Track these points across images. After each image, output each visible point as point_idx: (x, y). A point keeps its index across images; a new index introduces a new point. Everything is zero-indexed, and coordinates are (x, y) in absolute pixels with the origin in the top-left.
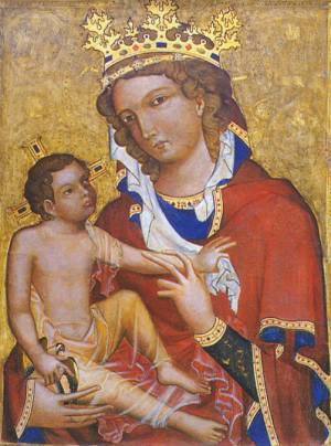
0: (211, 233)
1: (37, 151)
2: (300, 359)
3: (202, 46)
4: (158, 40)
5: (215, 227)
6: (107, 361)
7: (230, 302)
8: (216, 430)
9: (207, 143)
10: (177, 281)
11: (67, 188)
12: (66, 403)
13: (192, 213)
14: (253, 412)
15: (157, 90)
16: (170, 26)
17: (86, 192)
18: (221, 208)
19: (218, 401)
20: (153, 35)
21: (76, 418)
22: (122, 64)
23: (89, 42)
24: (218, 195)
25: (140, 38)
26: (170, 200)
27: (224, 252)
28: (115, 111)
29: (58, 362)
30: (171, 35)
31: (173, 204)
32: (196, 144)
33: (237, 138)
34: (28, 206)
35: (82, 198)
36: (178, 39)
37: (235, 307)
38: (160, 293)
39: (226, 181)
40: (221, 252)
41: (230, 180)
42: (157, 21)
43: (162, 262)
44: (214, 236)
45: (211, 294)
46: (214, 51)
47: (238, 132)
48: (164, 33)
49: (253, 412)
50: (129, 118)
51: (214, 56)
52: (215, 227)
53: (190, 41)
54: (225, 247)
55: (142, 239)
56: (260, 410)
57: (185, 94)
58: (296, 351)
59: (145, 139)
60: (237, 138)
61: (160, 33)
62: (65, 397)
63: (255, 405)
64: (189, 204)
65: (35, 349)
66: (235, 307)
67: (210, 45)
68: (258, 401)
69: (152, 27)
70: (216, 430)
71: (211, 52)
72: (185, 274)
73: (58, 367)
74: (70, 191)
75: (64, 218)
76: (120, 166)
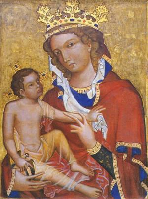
0: (95, 104)
1: (17, 67)
2: (134, 160)
3: (90, 20)
4: (71, 18)
5: (96, 101)
6: (48, 161)
7: (103, 135)
8: (97, 192)
9: (92, 64)
10: (79, 125)
11: (30, 84)
12: (29, 180)
13: (86, 95)
14: (113, 184)
16: (76, 12)
17: (38, 86)
18: (99, 93)
19: (98, 179)
20: (68, 16)
21: (34, 187)
22: (55, 28)
23: (40, 19)
24: (98, 87)
25: (63, 17)
26: (76, 89)
27: (100, 112)
28: (51, 49)
29: (26, 162)
30: (77, 16)
31: (78, 91)
32: (88, 64)
33: (106, 62)
34: (12, 92)
35: (36, 88)
36: (80, 17)
37: (105, 137)
38: (72, 131)
39: (101, 81)
40: (99, 112)
41: (103, 80)
42: (70, 10)
43: (72, 117)
44: (96, 105)
45: (94, 131)
46: (96, 23)
47: (106, 59)
48: (73, 15)
49: (113, 184)
50: (58, 53)
51: (95, 25)
52: (96, 101)
53: (85, 18)
54: (100, 110)
55: (64, 107)
56: (116, 183)
57: (83, 42)
58: (132, 156)
59: (65, 62)
60: (106, 62)
61: (71, 15)
62: (29, 177)
63: (114, 181)
64: (85, 91)
65: (16, 156)
66: (105, 137)
67: (94, 20)
68: (115, 179)
69: (68, 12)
70: (97, 192)
71: (94, 23)
72: (83, 122)
73: (26, 164)
74: (31, 85)
75: (29, 97)
76: (54, 74)
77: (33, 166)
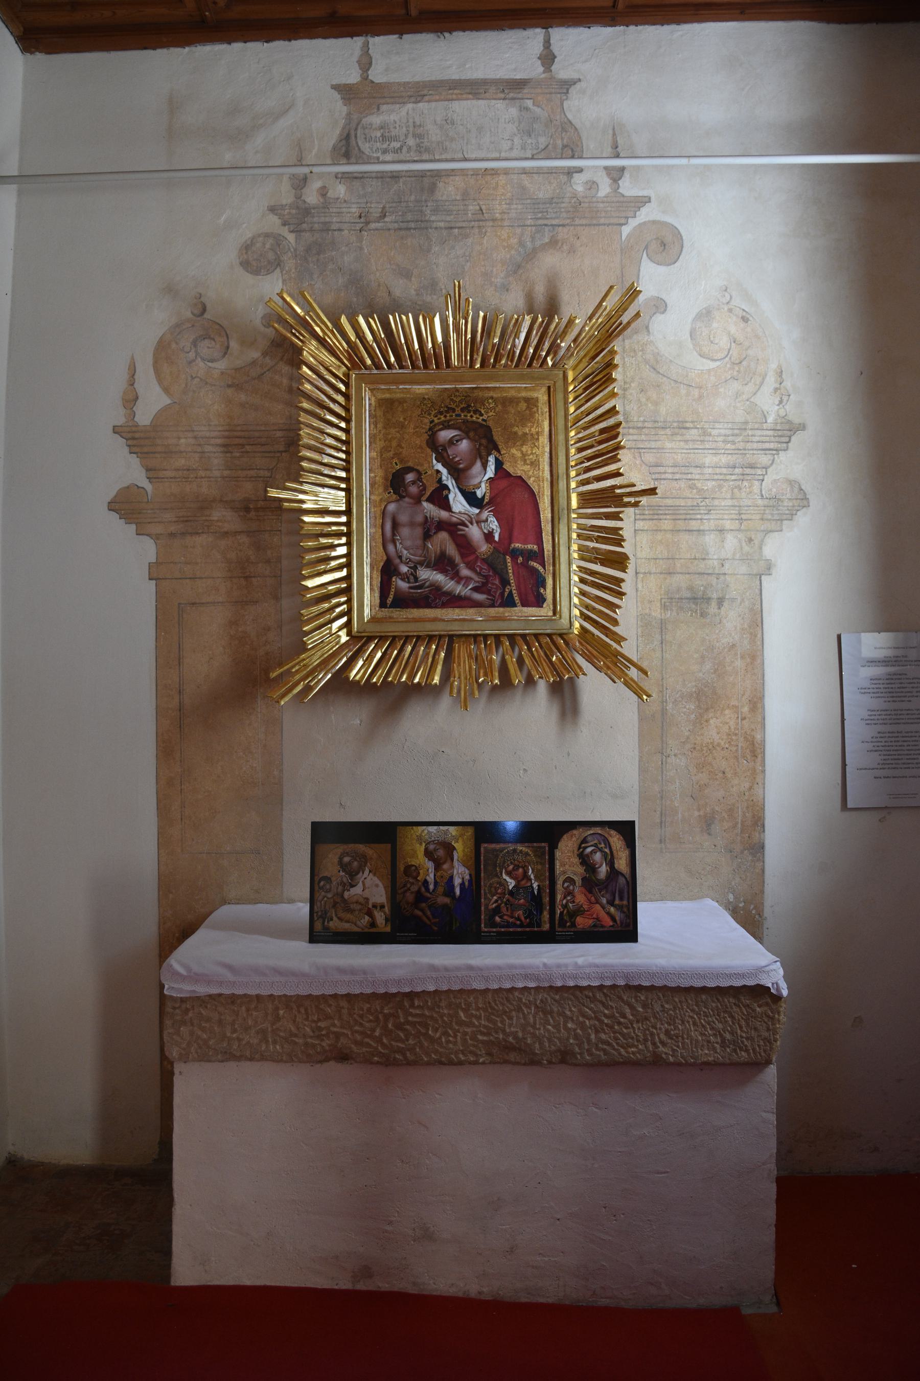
5: (486, 501)
7: (494, 537)
10: (467, 526)
12: (410, 588)
13: (475, 493)
21: (414, 595)
30: (462, 410)
37: (497, 538)
45: (484, 533)
52: (486, 501)
55: (450, 505)
57: (468, 438)
62: (412, 585)
65: (397, 561)
66: (497, 538)
68: (510, 586)
72: (472, 524)
76: (438, 472)
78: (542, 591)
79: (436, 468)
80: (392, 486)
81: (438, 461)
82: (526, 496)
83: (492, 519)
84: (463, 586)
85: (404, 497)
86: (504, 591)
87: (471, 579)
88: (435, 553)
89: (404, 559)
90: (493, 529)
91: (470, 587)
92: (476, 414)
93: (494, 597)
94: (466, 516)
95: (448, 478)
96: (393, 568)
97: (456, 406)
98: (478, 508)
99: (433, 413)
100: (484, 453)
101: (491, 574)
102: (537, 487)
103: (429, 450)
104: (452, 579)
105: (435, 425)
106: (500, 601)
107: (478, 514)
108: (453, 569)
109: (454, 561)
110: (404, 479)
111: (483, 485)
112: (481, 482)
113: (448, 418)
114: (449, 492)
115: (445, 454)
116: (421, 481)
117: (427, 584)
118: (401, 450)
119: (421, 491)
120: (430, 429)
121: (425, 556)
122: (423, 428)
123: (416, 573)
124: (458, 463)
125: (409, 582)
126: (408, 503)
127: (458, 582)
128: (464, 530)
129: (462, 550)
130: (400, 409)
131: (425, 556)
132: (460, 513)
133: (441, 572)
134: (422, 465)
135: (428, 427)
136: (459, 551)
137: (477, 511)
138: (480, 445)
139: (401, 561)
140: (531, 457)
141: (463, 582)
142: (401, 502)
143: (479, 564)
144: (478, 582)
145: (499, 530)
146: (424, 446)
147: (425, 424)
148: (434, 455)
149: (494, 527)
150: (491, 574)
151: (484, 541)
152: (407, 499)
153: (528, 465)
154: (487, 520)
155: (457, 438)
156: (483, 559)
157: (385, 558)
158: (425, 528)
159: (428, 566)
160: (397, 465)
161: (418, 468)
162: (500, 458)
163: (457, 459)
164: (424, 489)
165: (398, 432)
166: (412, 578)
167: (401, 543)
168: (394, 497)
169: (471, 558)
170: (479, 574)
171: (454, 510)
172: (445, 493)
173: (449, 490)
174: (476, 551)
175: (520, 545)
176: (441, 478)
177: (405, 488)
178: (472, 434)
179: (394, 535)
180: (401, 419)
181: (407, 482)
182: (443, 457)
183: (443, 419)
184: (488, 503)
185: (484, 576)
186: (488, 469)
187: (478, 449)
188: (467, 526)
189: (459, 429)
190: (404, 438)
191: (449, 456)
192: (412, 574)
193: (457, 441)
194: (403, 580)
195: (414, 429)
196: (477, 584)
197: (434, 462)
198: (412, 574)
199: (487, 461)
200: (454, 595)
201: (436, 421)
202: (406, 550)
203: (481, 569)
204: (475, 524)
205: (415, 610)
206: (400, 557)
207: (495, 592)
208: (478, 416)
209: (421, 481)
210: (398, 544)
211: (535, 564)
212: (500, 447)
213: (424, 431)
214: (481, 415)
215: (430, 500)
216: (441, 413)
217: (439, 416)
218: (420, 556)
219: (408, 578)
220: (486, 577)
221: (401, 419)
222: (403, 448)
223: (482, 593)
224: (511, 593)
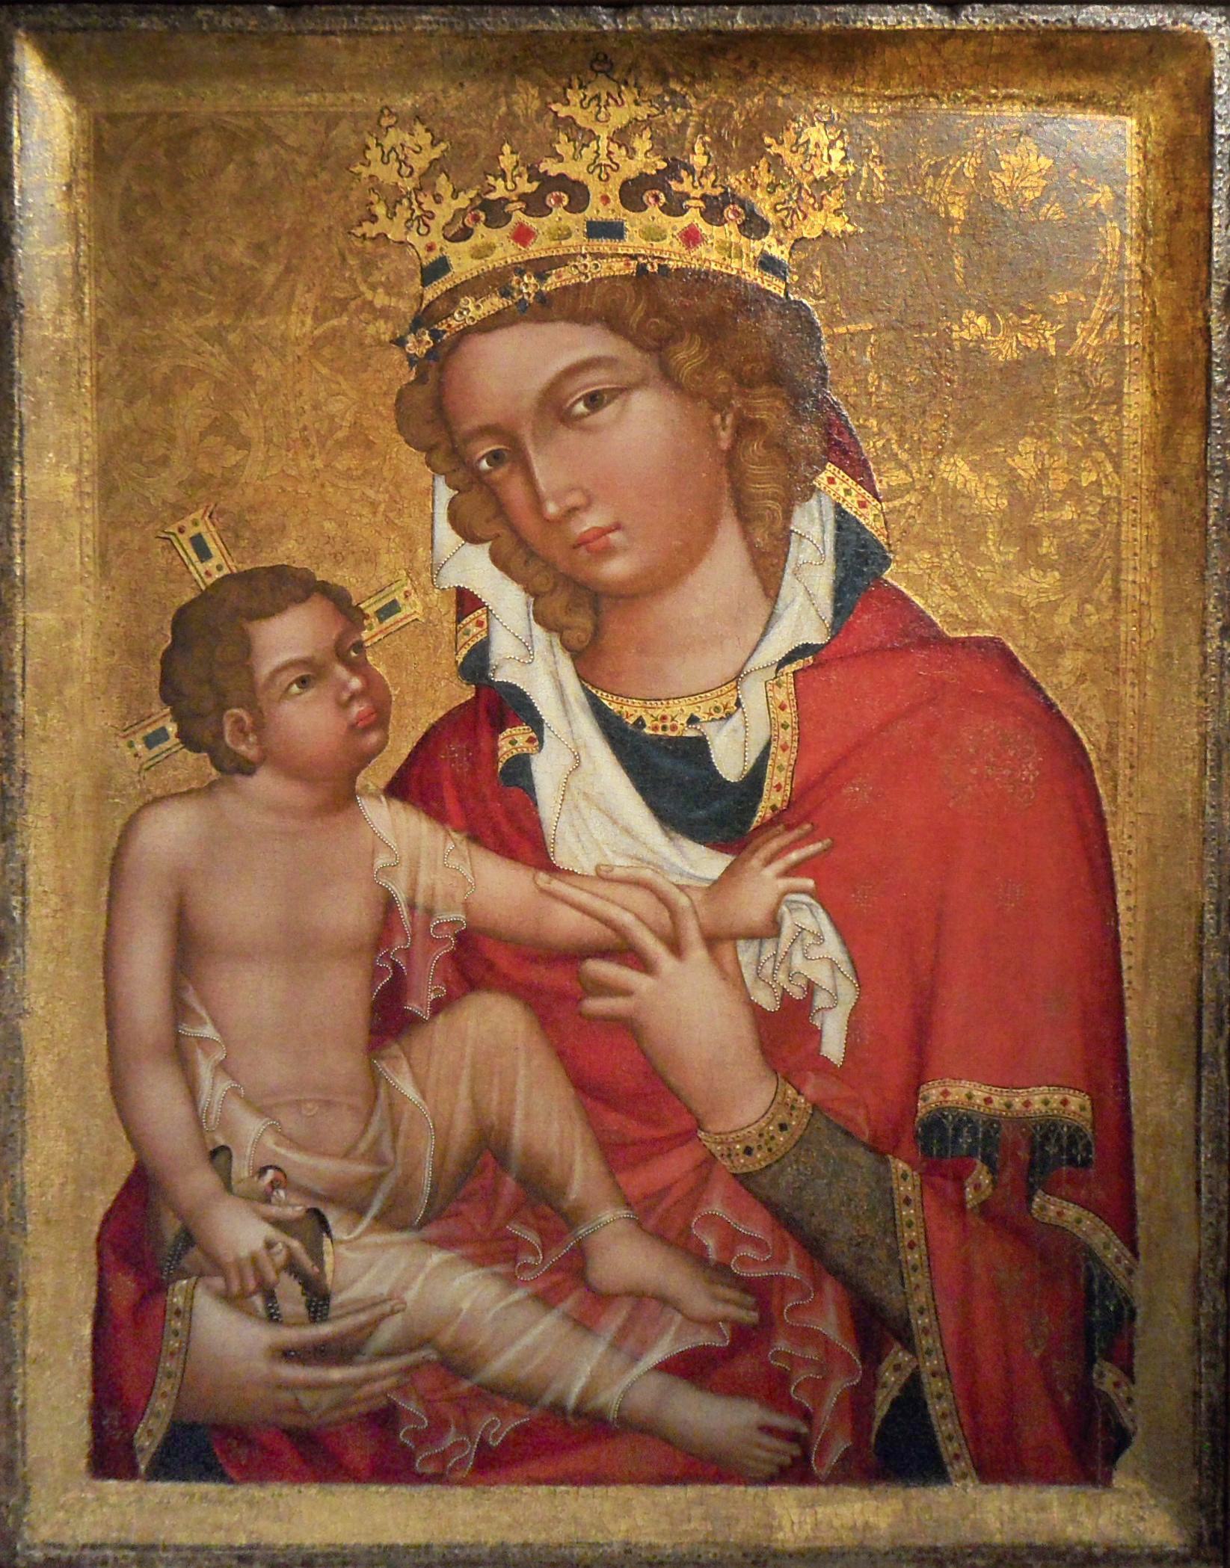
0: (763, 811)
1: (204, 554)
3: (729, 233)
4: (597, 211)
5: (772, 799)
6: (422, 1224)
7: (818, 1033)
8: (768, 1430)
9: (746, 535)
10: (641, 962)
12: (287, 1354)
13: (699, 748)
14: (891, 1379)
15: (93, 1547)
16: (631, 168)
17: (356, 683)
18: (787, 736)
19: (782, 1345)
20: (577, 195)
21: (307, 1399)
22: (476, 286)
23: (374, 218)
24: (784, 694)
25: (535, 205)
26: (630, 711)
27: (790, 872)
28: (451, 433)
29: (267, 1231)
30: (632, 194)
31: (640, 723)
32: (712, 525)
33: (844, 522)
34: (172, 729)
35: (344, 706)
36: (653, 211)
37: (833, 1046)
38: (596, 1005)
40: (787, 873)
41: (822, 647)
42: (587, 153)
43: (597, 905)
44: (768, 825)
45: (756, 1010)
47: (850, 505)
48: (613, 189)
49: (891, 1379)
50: (495, 457)
51: (767, 263)
53: (693, 217)
54: (794, 856)
55: (538, 823)
57: (669, 377)
59: (548, 522)
61: (595, 188)
62: (290, 1336)
63: (899, 1355)
64: (693, 720)
66: (833, 1046)
67: (754, 225)
68: (909, 1345)
69: (575, 170)
70: (768, 1430)
71: (757, 246)
72: (676, 947)
73: (269, 1245)
74: (303, 682)
75: (293, 769)
76: (466, 602)
77: (584, 689)
78: (1107, 1377)
79: (452, 578)
80: (170, 691)
81: (470, 537)
82: (1029, 772)
83: (806, 920)
84: (615, 1346)
85: (247, 768)
86: (871, 1381)
87: (664, 1301)
88: (443, 1136)
89: (241, 1169)
90: (811, 988)
91: (657, 1355)
92: (639, 207)
93: (807, 1416)
94: (640, 900)
95: (528, 646)
96: (171, 1228)
97: (595, 164)
98: (721, 846)
99: (443, 213)
100: (763, 484)
101: (791, 1270)
102: (1098, 715)
103: (411, 461)
104: (546, 1299)
105: (452, 296)
106: (840, 1445)
107: (718, 887)
108: (550, 1238)
109: (562, 1188)
110: (246, 649)
111: (754, 694)
112: (738, 677)
113: (536, 250)
114: (538, 740)
115: (515, 491)
116: (358, 667)
117: (386, 1334)
118: (233, 457)
119: (358, 729)
120: (425, 319)
121: (375, 1156)
122: (384, 313)
123: (318, 1257)
124: (597, 545)
125: (273, 1317)
126: (277, 809)
127: (584, 1324)
128: (627, 993)
129: (614, 1120)
130: (230, 178)
131: (375, 1156)
132: (603, 876)
133: (481, 1260)
134: (371, 557)
135: (406, 307)
136: (592, 1122)
137: (709, 864)
138: (745, 427)
139: (228, 1186)
140: (1068, 513)
141: (613, 1321)
142: (227, 801)
143: (717, 1208)
144: (711, 1323)
145: (849, 994)
146: (386, 430)
147: (392, 288)
148: (444, 494)
149: (821, 975)
150: (791, 1270)
151: (754, 1060)
152: (265, 783)
153: (1043, 565)
154: (773, 928)
155: (597, 379)
156: (744, 1179)
157: (124, 1161)
158: (377, 973)
159: (391, 1219)
160: (204, 554)
161: (343, 577)
162: (870, 519)
163: (591, 521)
164: (379, 718)
165: (217, 337)
166: (290, 1291)
167: (222, 1067)
168: (193, 765)
169: (675, 1166)
170: (719, 1272)
171: (561, 857)
172: (512, 741)
173: (536, 723)
174: (699, 1125)
175: (980, 1093)
176: (481, 652)
177: (251, 704)
178: (687, 355)
179: (179, 1010)
180: (238, 252)
181: (264, 670)
182: (501, 510)
183: (505, 251)
184: (780, 818)
185: (747, 1286)
186: (790, 587)
187: (731, 459)
188: (641, 962)
189: (613, 321)
190: (252, 379)
191: (537, 502)
192: (291, 1266)
193: (594, 401)
194: (234, 1300)
195: (319, 318)
196: (704, 1338)
197: (446, 535)
198: (291, 1266)
199: (784, 539)
200: (557, 1408)
201: (463, 263)
202: (262, 1111)
203: (732, 1239)
204: (698, 953)
205: (312, 1490)
206: (219, 1156)
207: (818, 1388)
208: (729, 233)
209: (358, 667)
210: (205, 1071)
211: (1072, 1212)
212: (869, 447)
213: (384, 329)
214: (754, 225)
215: (398, 789)
216: (494, 213)
217: (482, 234)
218: (347, 1155)
219: (270, 1296)
220: (759, 1292)
221: (238, 252)
222: (245, 444)
223: (735, 1389)
224: (911, 1398)
